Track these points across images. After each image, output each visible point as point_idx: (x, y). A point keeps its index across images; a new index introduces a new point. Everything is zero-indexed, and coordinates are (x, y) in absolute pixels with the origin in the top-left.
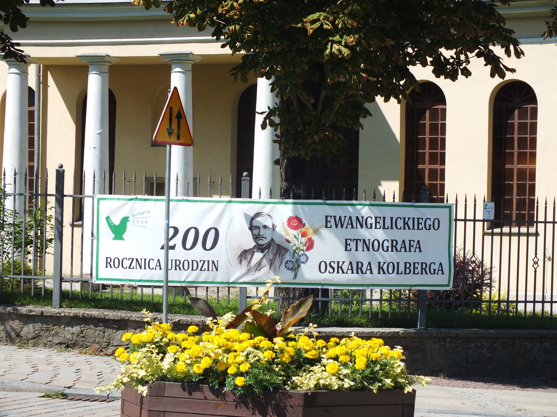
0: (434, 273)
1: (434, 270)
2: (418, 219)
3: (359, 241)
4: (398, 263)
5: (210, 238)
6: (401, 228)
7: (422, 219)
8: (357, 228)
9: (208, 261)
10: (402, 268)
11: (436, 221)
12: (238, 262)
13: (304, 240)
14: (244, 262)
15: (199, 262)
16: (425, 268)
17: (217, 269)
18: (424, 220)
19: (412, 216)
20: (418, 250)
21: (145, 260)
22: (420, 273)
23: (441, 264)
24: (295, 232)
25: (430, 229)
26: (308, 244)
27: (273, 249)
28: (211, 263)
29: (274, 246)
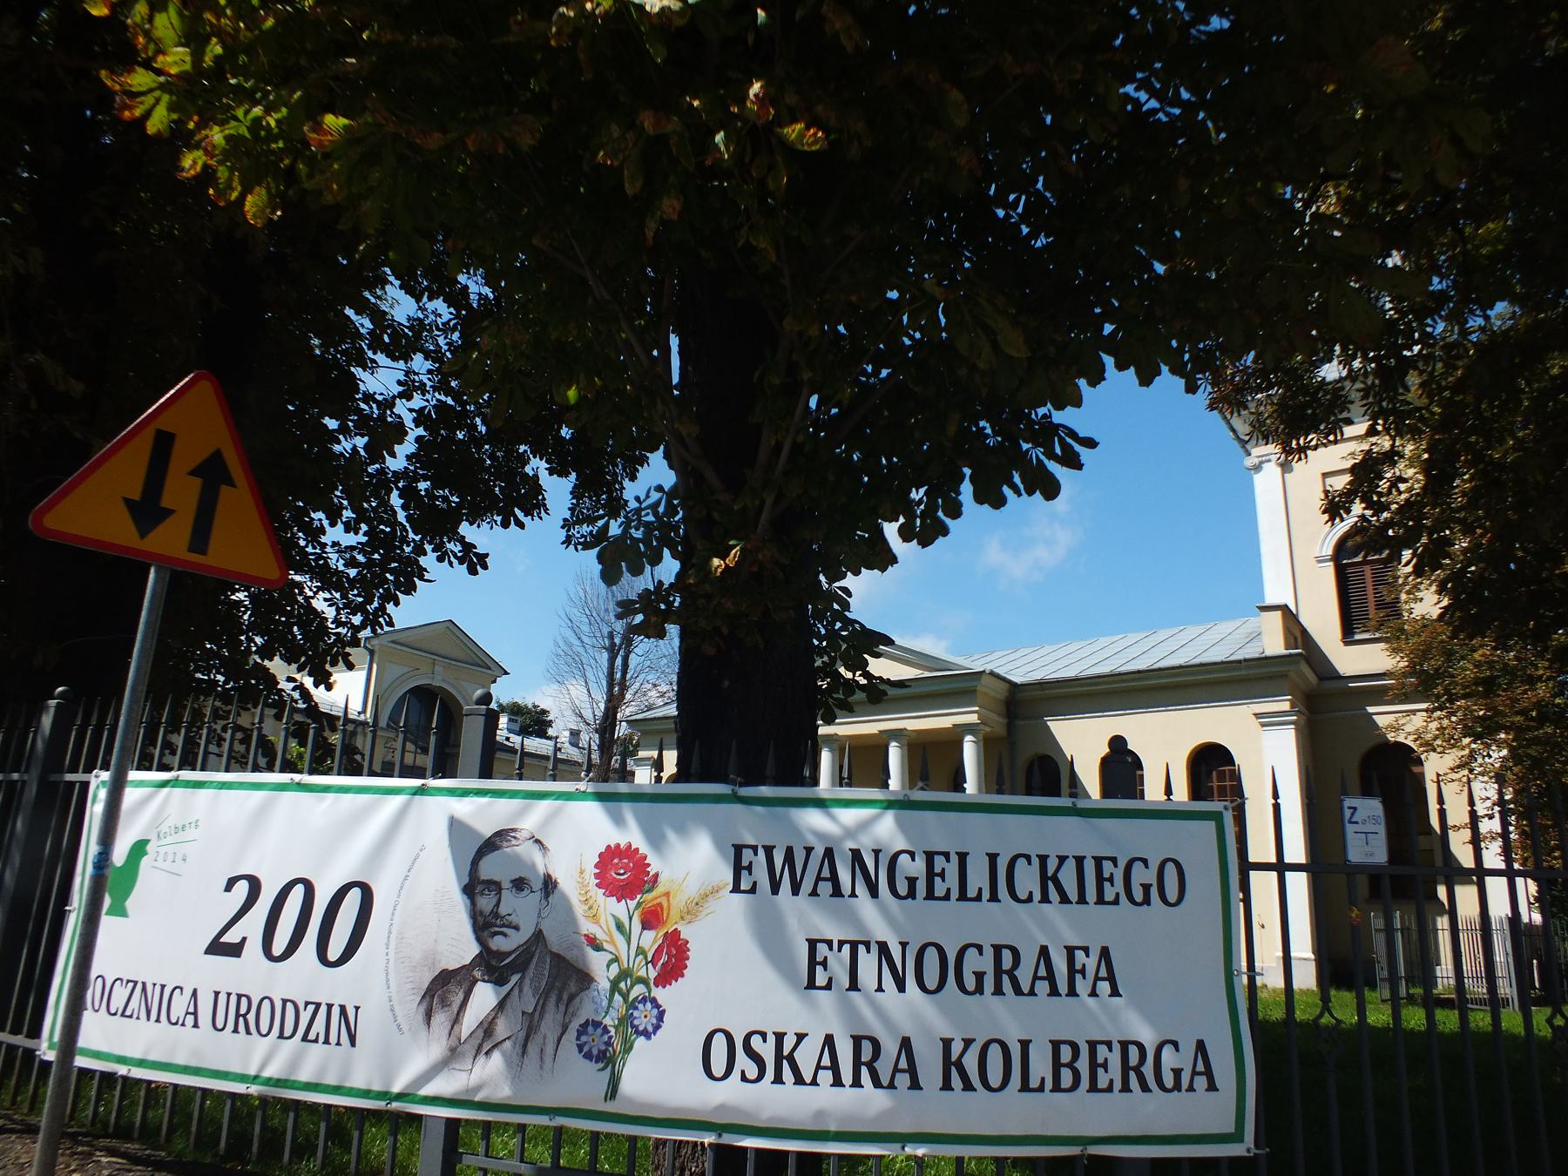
0: (1178, 1086)
1: (1177, 1073)
2: (1098, 861)
3: (862, 949)
4: (1025, 1044)
5: (331, 920)
6: (1030, 899)
7: (1114, 860)
8: (853, 895)
9: (330, 1006)
10: (1041, 1066)
11: (1170, 869)
12: (420, 1017)
13: (650, 940)
14: (441, 1019)
15: (301, 1007)
16: (1137, 1068)
17: (353, 1044)
18: (1122, 864)
19: (1072, 851)
20: (1104, 987)
21: (163, 987)
22: (1118, 1085)
23: (1201, 1046)
24: (619, 909)
25: (1147, 901)
26: (664, 958)
27: (539, 971)
28: (336, 1011)
29: (541, 960)
